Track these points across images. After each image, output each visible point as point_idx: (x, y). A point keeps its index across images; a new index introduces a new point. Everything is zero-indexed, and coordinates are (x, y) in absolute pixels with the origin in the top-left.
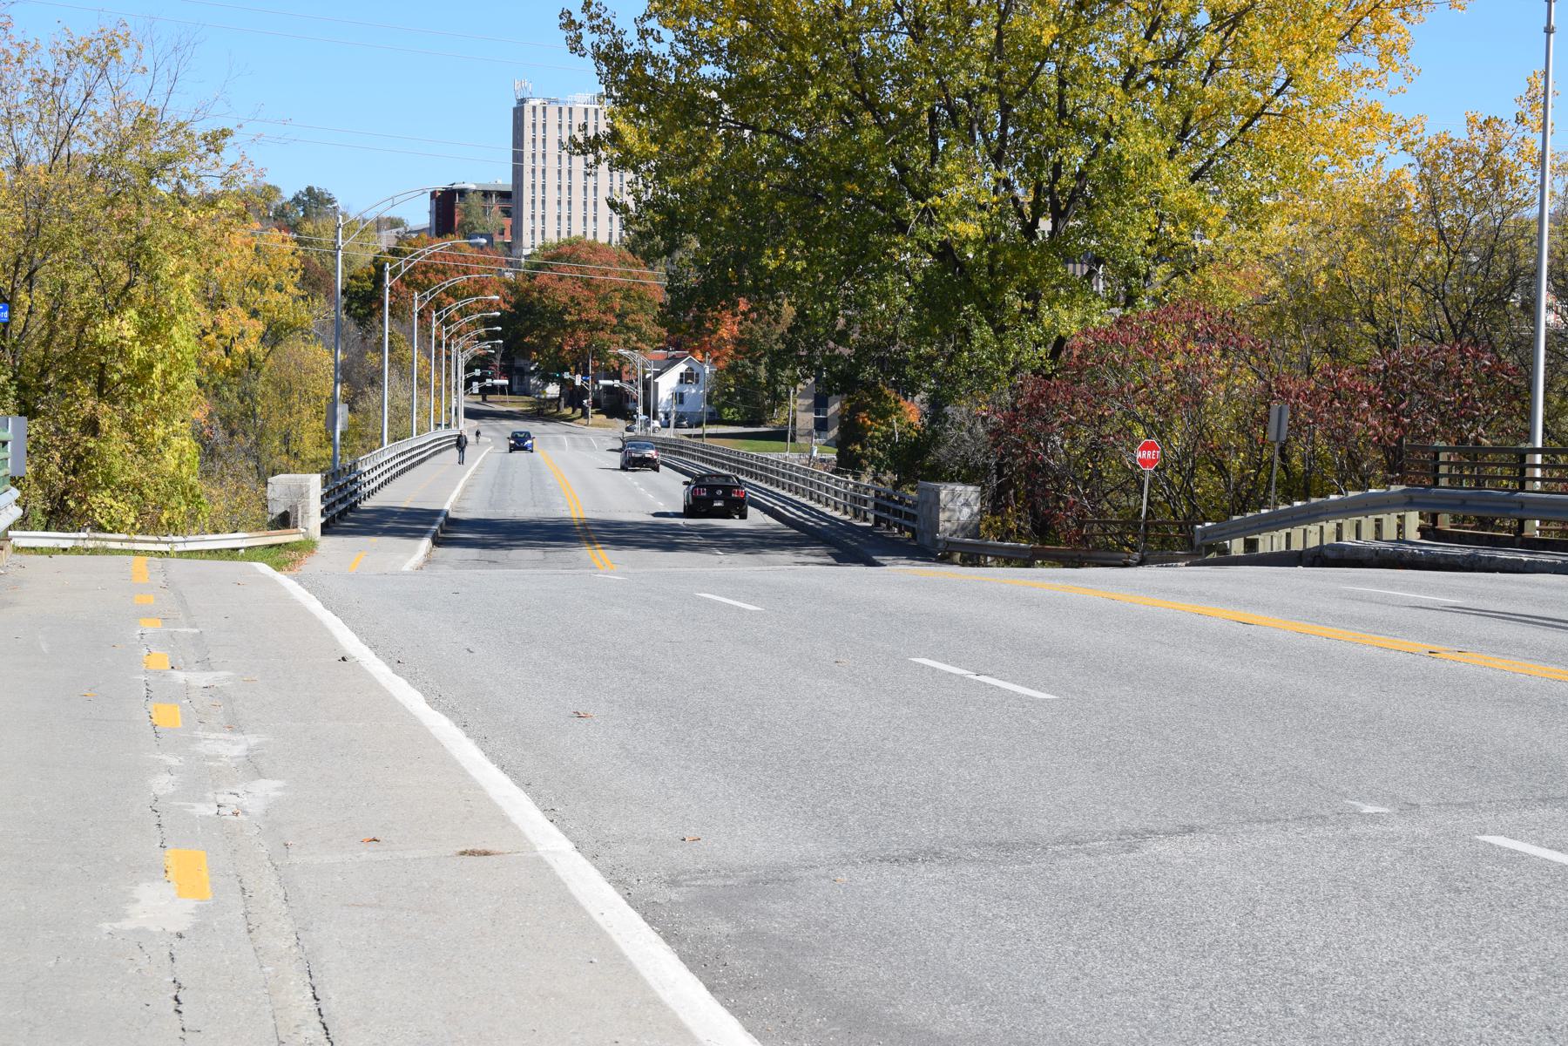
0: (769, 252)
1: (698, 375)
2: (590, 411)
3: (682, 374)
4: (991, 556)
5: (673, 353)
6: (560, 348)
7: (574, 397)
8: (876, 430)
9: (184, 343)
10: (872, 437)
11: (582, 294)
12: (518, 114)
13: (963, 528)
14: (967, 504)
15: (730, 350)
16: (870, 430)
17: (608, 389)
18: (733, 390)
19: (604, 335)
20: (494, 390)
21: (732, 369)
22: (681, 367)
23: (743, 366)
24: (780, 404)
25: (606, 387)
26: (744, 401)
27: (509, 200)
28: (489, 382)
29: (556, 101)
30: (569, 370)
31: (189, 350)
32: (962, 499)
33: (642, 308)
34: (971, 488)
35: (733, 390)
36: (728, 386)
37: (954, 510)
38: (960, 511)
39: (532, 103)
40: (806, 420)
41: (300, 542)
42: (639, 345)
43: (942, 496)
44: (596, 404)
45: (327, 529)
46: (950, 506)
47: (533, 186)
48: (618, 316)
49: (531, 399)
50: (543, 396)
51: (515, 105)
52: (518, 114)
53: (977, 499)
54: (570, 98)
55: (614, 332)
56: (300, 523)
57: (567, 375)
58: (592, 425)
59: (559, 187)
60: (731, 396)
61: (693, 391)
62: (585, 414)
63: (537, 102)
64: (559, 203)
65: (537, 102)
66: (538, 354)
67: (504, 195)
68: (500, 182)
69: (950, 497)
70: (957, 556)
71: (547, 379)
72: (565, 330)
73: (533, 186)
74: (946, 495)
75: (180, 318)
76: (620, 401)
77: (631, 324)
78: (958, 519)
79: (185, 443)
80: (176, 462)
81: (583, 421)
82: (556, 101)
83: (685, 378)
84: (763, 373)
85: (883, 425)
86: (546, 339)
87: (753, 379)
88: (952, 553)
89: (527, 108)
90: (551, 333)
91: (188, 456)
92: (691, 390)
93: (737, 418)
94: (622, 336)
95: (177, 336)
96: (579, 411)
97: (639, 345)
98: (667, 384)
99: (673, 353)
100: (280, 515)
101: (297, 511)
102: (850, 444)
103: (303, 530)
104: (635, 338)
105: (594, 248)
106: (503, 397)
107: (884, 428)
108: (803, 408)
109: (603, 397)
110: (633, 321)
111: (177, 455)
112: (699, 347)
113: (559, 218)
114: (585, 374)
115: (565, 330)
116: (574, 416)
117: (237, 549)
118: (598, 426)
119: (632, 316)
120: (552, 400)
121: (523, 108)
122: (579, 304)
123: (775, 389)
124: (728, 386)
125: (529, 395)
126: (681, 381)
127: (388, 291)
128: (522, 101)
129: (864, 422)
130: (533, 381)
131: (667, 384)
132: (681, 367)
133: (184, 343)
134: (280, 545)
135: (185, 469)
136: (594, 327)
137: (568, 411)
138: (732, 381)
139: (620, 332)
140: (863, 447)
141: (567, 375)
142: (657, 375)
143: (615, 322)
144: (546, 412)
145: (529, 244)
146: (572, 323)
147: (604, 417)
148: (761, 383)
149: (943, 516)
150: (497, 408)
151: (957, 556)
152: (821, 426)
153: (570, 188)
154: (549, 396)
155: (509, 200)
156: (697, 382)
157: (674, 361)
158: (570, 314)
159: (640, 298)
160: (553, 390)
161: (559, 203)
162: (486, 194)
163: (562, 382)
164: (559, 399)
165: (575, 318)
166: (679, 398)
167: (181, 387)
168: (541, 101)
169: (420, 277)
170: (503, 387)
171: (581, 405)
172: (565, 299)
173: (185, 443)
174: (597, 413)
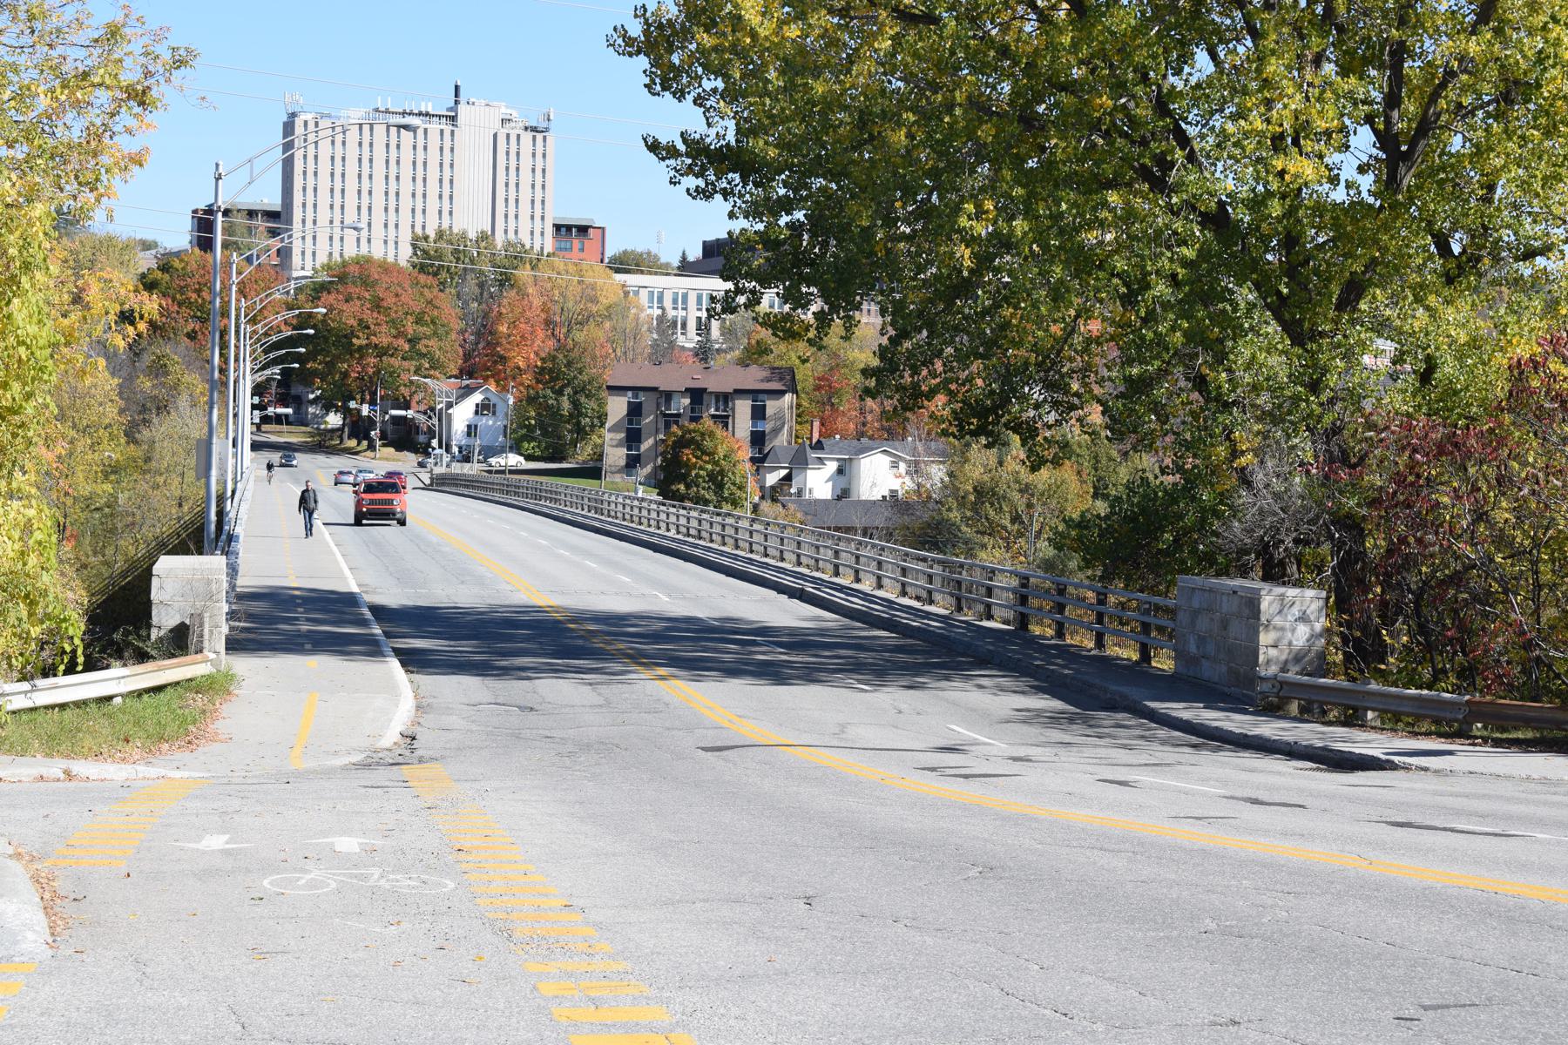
0: (970, 207)
1: (494, 405)
2: (378, 443)
3: (477, 405)
4: (1373, 710)
5: (468, 382)
6: (345, 375)
7: (359, 428)
8: (701, 468)
9: (33, 329)
10: (698, 476)
11: (370, 317)
12: (289, 128)
13: (1298, 658)
14: (1303, 618)
15: (527, 379)
16: (695, 468)
17: (395, 419)
18: (533, 422)
19: (396, 362)
20: (279, 419)
21: (531, 400)
22: (477, 397)
23: (545, 397)
24: (583, 439)
25: (393, 418)
26: (545, 433)
27: (277, 219)
28: (271, 411)
29: (329, 116)
30: (354, 399)
31: (42, 342)
32: (1296, 611)
33: (435, 333)
34: (1310, 593)
35: (533, 422)
36: (528, 419)
37: (1282, 629)
38: (1293, 630)
39: (303, 117)
40: (616, 456)
41: (210, 676)
42: (432, 372)
43: (1264, 606)
44: (383, 436)
45: (235, 645)
46: (1277, 621)
47: (304, 205)
48: (410, 341)
49: (308, 429)
50: (323, 427)
51: (285, 119)
52: (289, 128)
53: (1320, 610)
54: (343, 113)
55: (404, 359)
56: (206, 644)
57: (353, 405)
58: (380, 459)
59: (332, 207)
60: (530, 428)
61: (491, 422)
62: (371, 447)
63: (309, 117)
64: (414, 195)
65: (309, 117)
66: (322, 381)
67: (272, 215)
68: (266, 201)
69: (1276, 607)
70: (1294, 708)
71: (328, 407)
72: (351, 355)
73: (304, 205)
74: (1270, 604)
75: (25, 281)
76: (409, 432)
77: (424, 350)
78: (1290, 644)
79: (32, 513)
80: (17, 546)
81: (369, 453)
82: (329, 116)
83: (481, 409)
84: (566, 405)
85: (708, 463)
86: (331, 366)
87: (555, 413)
88: (1285, 701)
89: (299, 123)
90: (338, 358)
91: (38, 536)
92: (487, 422)
93: (538, 453)
94: (414, 363)
95: (20, 317)
96: (365, 443)
97: (432, 372)
98: (463, 414)
99: (468, 382)
100: (171, 631)
101: (201, 625)
102: (673, 484)
103: (212, 656)
104: (427, 366)
105: (386, 268)
106: (278, 427)
107: (709, 467)
108: (614, 443)
109: (390, 428)
110: (427, 346)
111: (16, 534)
112: (493, 376)
113: (413, 211)
114: (372, 403)
115: (351, 355)
116: (359, 449)
117: (109, 698)
118: (387, 459)
119: (424, 342)
120: (333, 431)
121: (293, 122)
122: (368, 328)
123: (579, 423)
124: (528, 419)
125: (307, 425)
126: (476, 413)
127: (234, 288)
128: (293, 115)
129: (688, 459)
130: (311, 410)
131: (463, 414)
132: (477, 397)
133: (33, 329)
134: (178, 683)
135: (33, 560)
136: (382, 352)
137: (352, 443)
138: (533, 414)
139: (412, 359)
140: (688, 487)
141: (353, 405)
142: (449, 405)
143: (407, 347)
144: (327, 444)
145: (304, 267)
146: (361, 348)
147: (391, 450)
148: (562, 416)
149: (1265, 638)
150: (273, 438)
151: (1294, 708)
152: (633, 463)
153: (342, 207)
154: (329, 427)
155: (277, 219)
156: (494, 414)
157: (467, 392)
158: (358, 338)
159: (433, 322)
160: (334, 420)
161: (414, 195)
162: (251, 214)
163: (346, 411)
164: (341, 429)
165: (365, 342)
166: (471, 430)
167: (30, 408)
168: (313, 115)
169: (194, 296)
170: (287, 416)
171: (367, 437)
172: (353, 322)
173: (32, 513)
174: (384, 445)
